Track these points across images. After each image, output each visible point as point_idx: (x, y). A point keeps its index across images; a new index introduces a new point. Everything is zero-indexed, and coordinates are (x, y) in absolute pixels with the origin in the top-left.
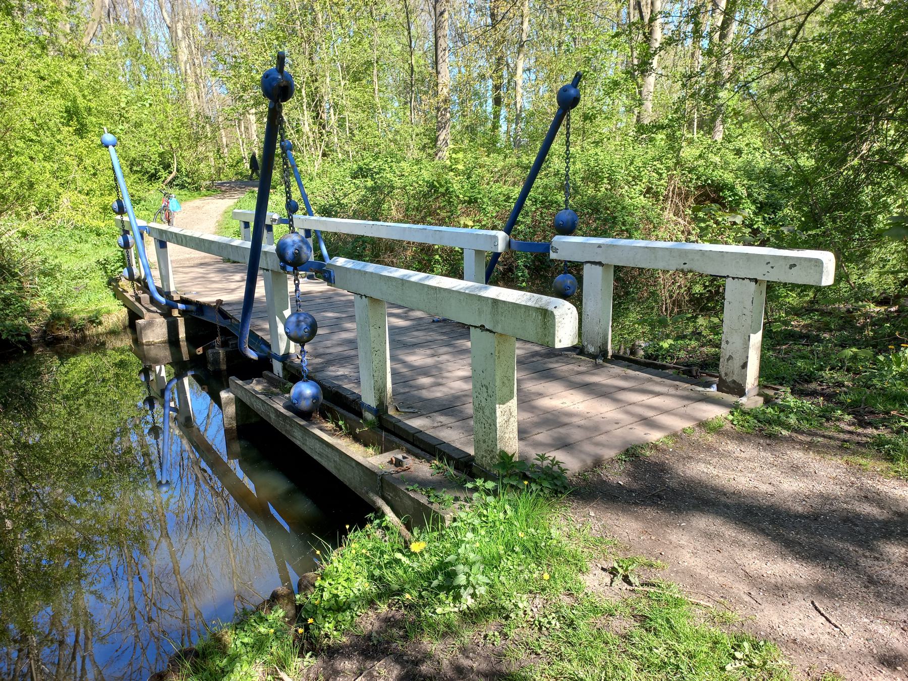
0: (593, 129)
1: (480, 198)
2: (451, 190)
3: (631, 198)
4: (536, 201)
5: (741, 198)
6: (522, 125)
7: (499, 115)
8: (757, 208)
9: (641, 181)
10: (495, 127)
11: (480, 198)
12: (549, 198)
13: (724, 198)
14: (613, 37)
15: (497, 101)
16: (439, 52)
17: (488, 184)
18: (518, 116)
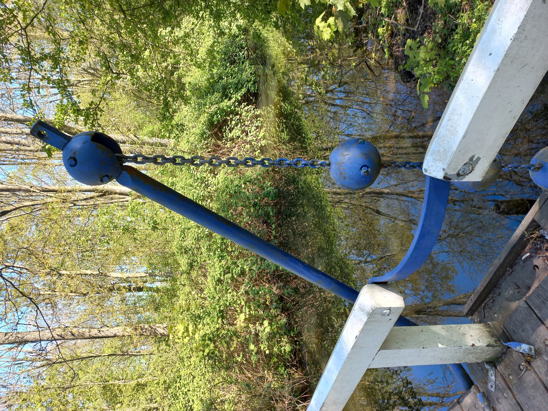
0: (163, 224)
1: (220, 307)
2: (211, 336)
3: (218, 183)
4: (222, 256)
5: (219, 109)
6: (157, 272)
7: (149, 288)
8: (226, 98)
9: (205, 178)
10: (158, 290)
11: (220, 307)
12: (219, 245)
13: (219, 121)
14: (103, 204)
15: (140, 289)
16: (100, 335)
17: (205, 299)
18: (151, 275)
